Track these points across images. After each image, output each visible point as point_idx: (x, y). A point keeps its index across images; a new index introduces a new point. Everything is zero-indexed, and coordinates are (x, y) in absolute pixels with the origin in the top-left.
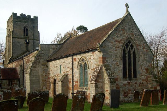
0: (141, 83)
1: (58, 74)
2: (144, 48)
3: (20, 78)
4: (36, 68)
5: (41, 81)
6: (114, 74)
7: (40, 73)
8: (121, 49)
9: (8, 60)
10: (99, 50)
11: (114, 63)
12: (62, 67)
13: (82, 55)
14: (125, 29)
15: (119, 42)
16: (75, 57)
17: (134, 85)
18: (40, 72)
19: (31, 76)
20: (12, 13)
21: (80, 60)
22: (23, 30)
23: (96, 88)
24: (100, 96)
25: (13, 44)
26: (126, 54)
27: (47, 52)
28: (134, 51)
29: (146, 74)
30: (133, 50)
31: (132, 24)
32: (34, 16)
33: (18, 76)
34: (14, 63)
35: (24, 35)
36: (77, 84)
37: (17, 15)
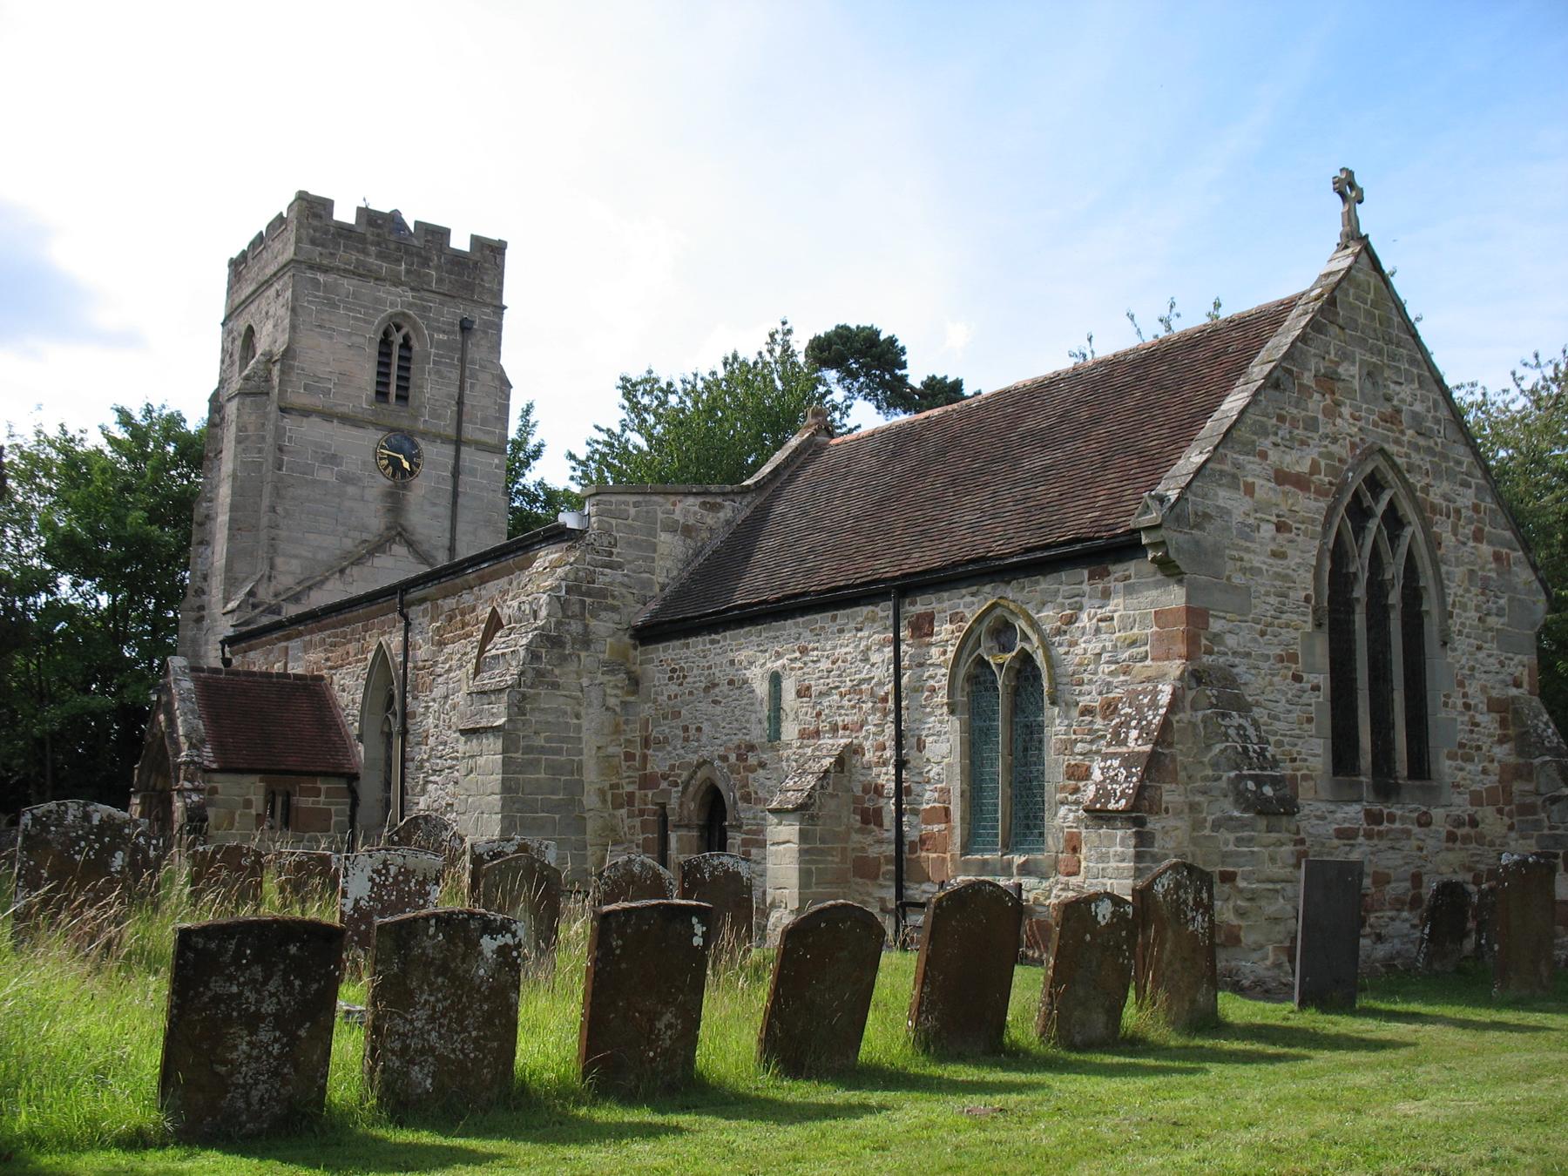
0: (1459, 823)
1: (751, 748)
2: (1478, 536)
3: (362, 772)
4: (555, 686)
5: (590, 800)
7: (585, 735)
8: (1317, 543)
11: (1268, 657)
12: (789, 687)
14: (1339, 379)
15: (1300, 482)
17: (1408, 833)
18: (585, 723)
22: (372, 351)
23: (1139, 857)
24: (1178, 885)
26: (1352, 584)
27: (637, 559)
28: (1410, 556)
30: (1403, 550)
31: (1390, 342)
34: (300, 634)
35: (378, 393)
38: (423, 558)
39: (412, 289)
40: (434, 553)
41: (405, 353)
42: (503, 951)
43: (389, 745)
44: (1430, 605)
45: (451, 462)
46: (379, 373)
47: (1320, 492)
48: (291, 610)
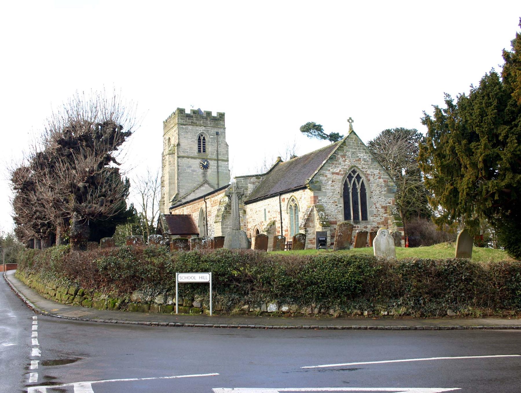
1: (262, 222)
2: (380, 178)
6: (330, 216)
9: (170, 199)
10: (309, 188)
13: (291, 194)
15: (337, 174)
16: (283, 196)
19: (224, 226)
20: (176, 109)
21: (289, 201)
22: (197, 142)
24: (300, 236)
25: (178, 169)
29: (385, 215)
32: (218, 113)
33: (195, 228)
34: (186, 206)
35: (199, 151)
36: (287, 233)
37: (186, 112)
38: (212, 186)
39: (204, 127)
40: (214, 185)
41: (204, 141)
42: (205, 241)
43: (205, 227)
44: (367, 191)
45: (216, 165)
46: (199, 149)
47: (342, 175)
48: (184, 201)
